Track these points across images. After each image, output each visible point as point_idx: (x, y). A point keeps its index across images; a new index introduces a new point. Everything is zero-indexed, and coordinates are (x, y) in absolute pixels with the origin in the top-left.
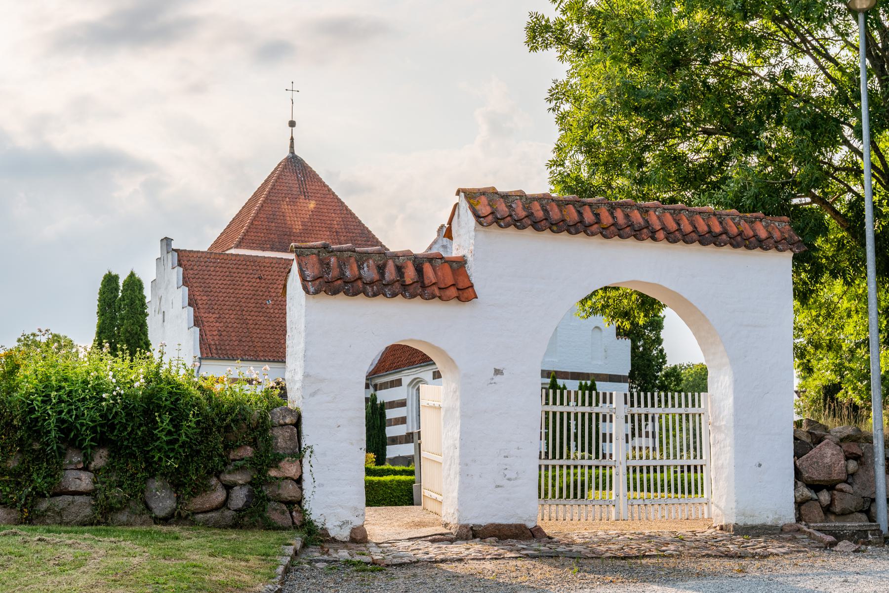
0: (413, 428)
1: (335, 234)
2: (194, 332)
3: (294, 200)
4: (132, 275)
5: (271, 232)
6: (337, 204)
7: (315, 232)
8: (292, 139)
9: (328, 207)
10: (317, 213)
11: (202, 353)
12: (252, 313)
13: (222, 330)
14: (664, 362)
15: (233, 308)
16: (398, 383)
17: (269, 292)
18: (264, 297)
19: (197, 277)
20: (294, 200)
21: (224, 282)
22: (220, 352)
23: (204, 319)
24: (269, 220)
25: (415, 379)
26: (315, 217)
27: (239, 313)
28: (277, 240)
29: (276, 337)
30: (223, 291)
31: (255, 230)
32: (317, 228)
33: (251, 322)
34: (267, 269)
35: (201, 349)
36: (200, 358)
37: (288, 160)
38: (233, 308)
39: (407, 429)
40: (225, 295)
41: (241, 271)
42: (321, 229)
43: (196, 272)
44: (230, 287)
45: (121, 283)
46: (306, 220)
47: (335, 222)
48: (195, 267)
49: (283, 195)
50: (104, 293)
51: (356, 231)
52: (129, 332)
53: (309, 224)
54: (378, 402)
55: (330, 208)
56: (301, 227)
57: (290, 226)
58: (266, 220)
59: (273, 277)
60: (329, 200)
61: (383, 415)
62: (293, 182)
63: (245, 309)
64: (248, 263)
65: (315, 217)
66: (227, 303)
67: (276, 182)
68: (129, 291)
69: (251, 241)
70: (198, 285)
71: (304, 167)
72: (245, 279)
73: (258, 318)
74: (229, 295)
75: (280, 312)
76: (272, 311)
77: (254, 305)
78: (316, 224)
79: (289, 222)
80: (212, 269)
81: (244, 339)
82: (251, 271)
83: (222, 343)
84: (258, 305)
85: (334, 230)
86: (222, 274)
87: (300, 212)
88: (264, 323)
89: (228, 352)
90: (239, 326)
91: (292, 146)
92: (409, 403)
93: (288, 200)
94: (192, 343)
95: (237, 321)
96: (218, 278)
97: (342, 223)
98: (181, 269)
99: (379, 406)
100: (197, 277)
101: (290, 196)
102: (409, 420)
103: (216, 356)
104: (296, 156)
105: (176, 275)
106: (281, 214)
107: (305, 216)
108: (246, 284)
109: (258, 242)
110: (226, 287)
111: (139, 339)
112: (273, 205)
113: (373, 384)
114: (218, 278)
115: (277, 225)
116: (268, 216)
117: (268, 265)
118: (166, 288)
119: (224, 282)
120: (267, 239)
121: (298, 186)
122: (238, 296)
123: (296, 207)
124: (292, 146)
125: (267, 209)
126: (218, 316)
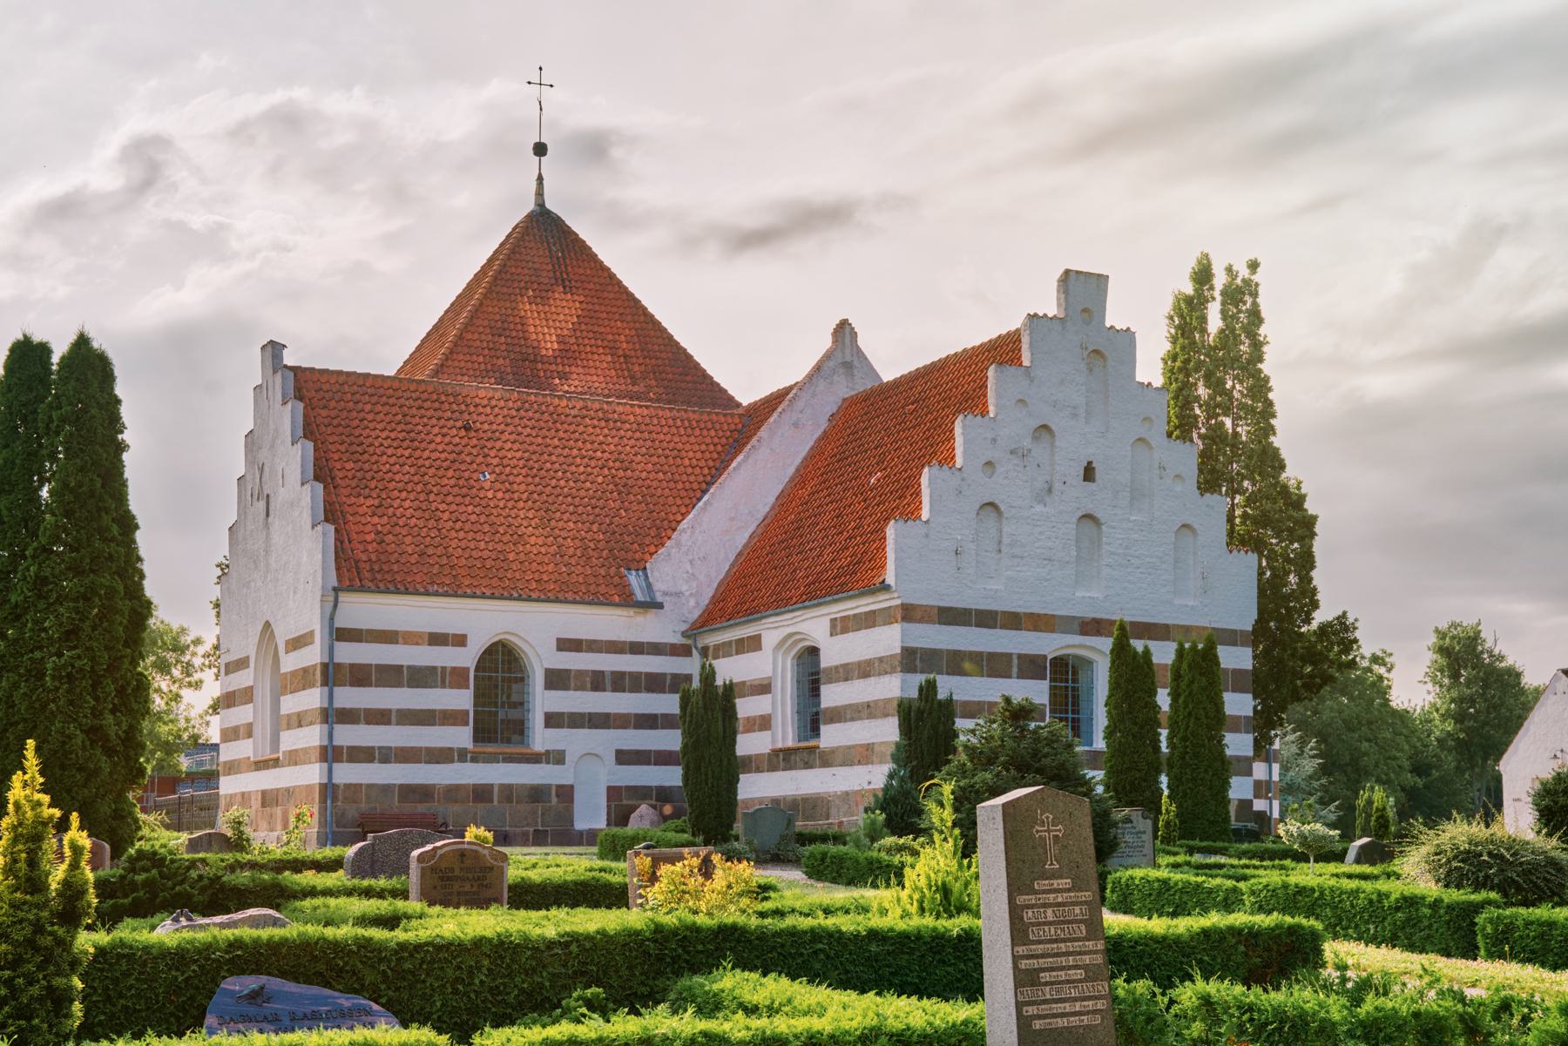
0: (784, 738)
1: (622, 359)
2: (324, 534)
3: (544, 294)
4: (82, 342)
5: (498, 354)
6: (627, 304)
7: (583, 356)
8: (540, 179)
9: (609, 309)
10: (587, 320)
11: (340, 577)
12: (450, 498)
13: (385, 531)
14: (1315, 605)
15: (409, 487)
16: (754, 643)
17: (486, 456)
18: (475, 465)
19: (335, 422)
20: (544, 294)
21: (393, 435)
22: (379, 576)
23: (348, 509)
24: (495, 331)
25: (791, 635)
26: (583, 327)
27: (422, 497)
28: (509, 370)
29: (499, 547)
30: (390, 451)
31: (466, 350)
32: (588, 349)
33: (446, 516)
34: (481, 410)
35: (338, 569)
36: (335, 589)
37: (530, 216)
38: (409, 487)
39: (774, 741)
40: (392, 460)
41: (429, 414)
42: (594, 350)
43: (333, 413)
44: (405, 444)
45: (55, 359)
46: (566, 332)
47: (623, 338)
48: (333, 404)
49: (522, 284)
50: (10, 390)
51: (663, 355)
52: (72, 491)
53: (573, 340)
54: (719, 682)
55: (614, 310)
56: (556, 346)
57: (535, 344)
58: (488, 331)
59: (494, 427)
60: (611, 296)
61: (729, 712)
62: (542, 260)
63: (435, 490)
64: (443, 398)
65: (583, 327)
66: (397, 478)
67: (509, 259)
68: (73, 383)
69: (458, 370)
70: (336, 438)
71: (564, 232)
72: (436, 430)
73: (462, 509)
74: (401, 460)
75: (507, 496)
76: (490, 495)
77: (452, 482)
78: (586, 341)
79: (534, 337)
80: (368, 407)
81: (430, 551)
82: (449, 414)
83: (383, 558)
84: (461, 482)
85: (621, 353)
86: (388, 419)
87: (555, 317)
88: (473, 518)
89: (397, 576)
90: (421, 523)
91: (540, 193)
92: (777, 685)
93: (531, 293)
94: (320, 556)
95: (418, 514)
96: (380, 426)
97: (636, 339)
98: (301, 406)
99: (720, 691)
100: (335, 422)
101: (535, 286)
102: (777, 722)
103: (370, 584)
104: (549, 212)
105: (286, 417)
106: (518, 320)
107: (563, 324)
108: (438, 439)
109: (471, 372)
110: (395, 444)
111: (99, 509)
112: (502, 303)
113: (700, 646)
114: (380, 426)
115: (509, 340)
116: (493, 324)
117: (485, 402)
118: (272, 447)
119: (393, 435)
120: (489, 367)
121: (550, 267)
122: (420, 462)
123: (547, 308)
124: (540, 193)
125: (490, 309)
126: (376, 502)
